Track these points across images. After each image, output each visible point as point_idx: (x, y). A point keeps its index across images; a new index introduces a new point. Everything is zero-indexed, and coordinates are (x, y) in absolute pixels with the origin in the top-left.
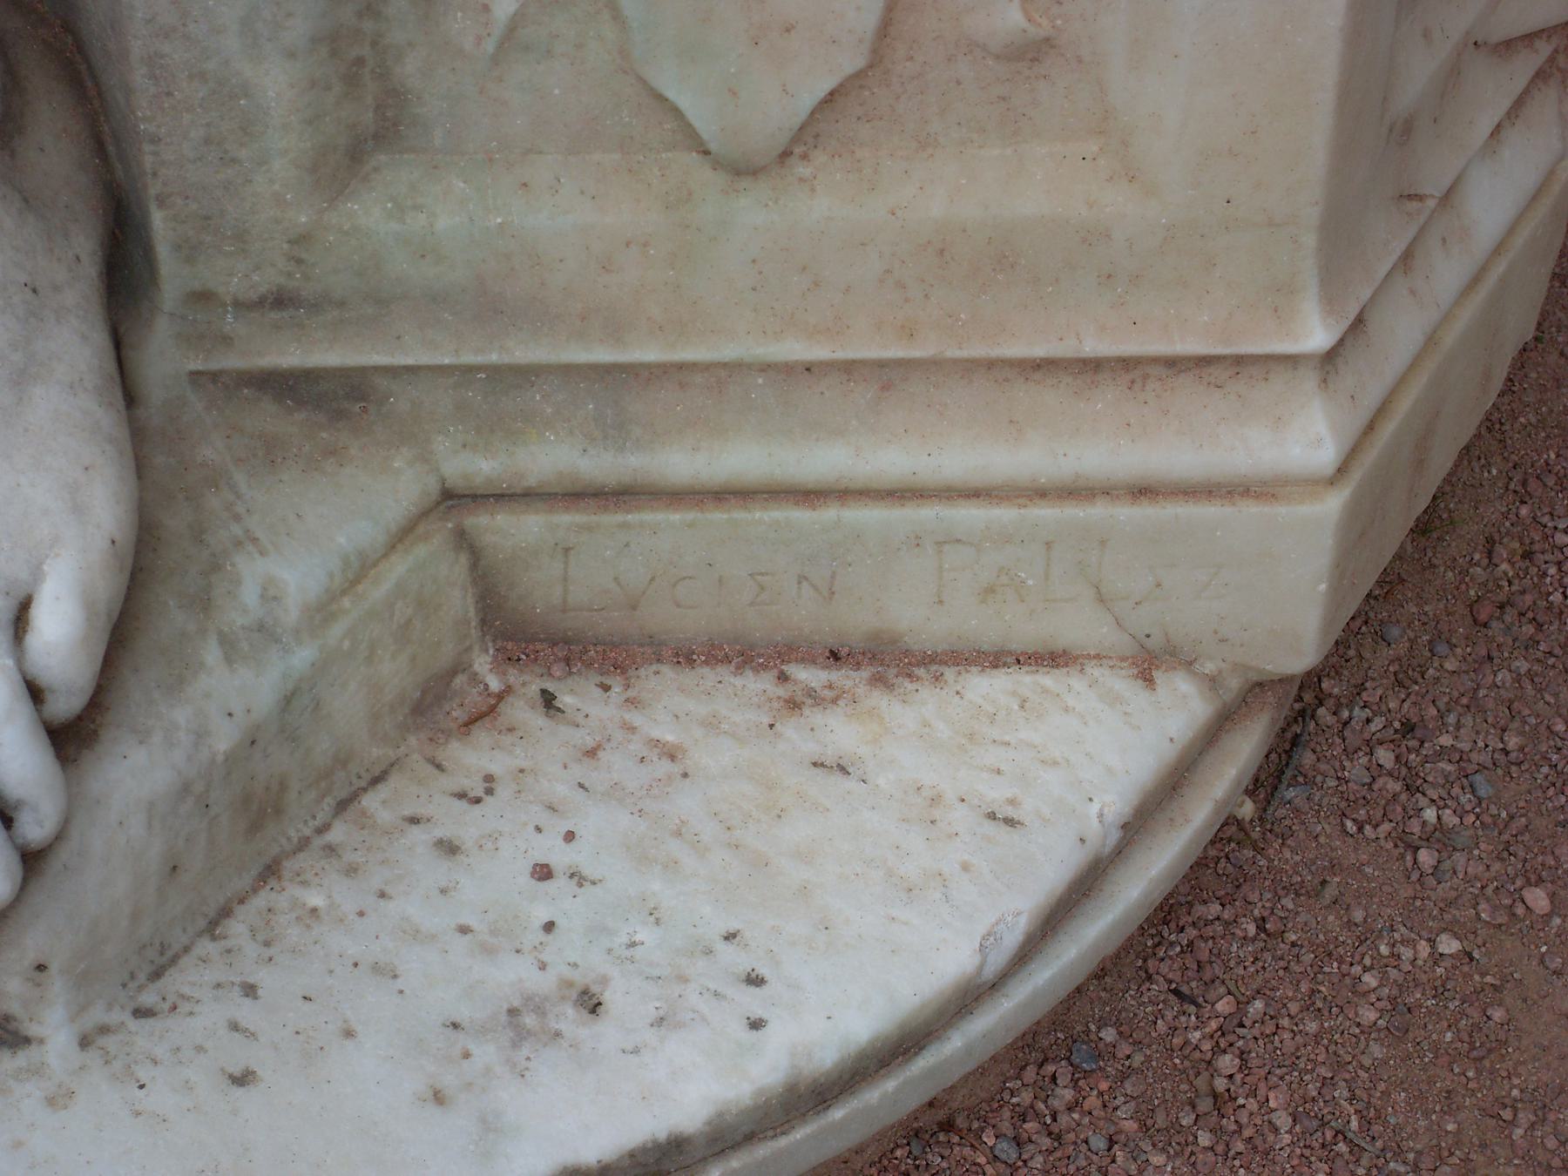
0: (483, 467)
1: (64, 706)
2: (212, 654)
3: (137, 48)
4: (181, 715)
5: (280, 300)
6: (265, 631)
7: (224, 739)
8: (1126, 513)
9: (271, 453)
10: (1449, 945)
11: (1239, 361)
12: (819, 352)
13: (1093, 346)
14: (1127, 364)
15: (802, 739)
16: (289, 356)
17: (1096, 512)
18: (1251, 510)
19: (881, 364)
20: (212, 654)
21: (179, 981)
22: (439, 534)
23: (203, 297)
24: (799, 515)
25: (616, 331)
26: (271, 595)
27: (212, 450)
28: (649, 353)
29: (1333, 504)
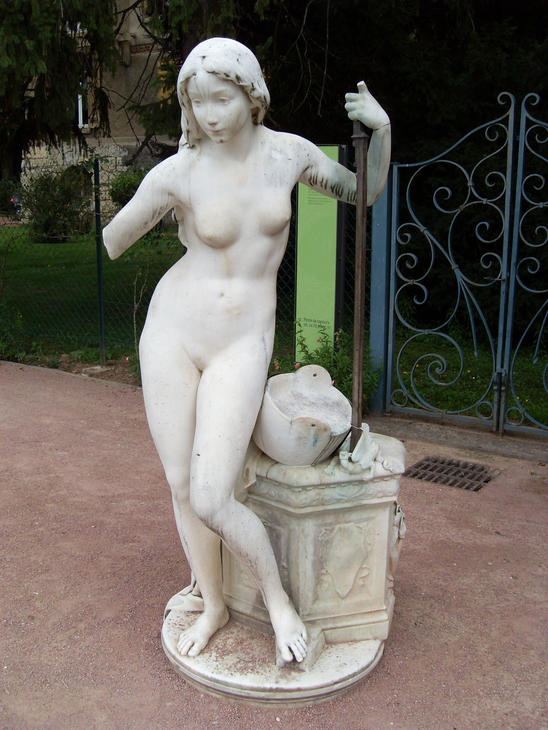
0: (325, 627)
1: (306, 641)
2: (312, 640)
3: (300, 593)
5: (309, 615)
8: (373, 624)
10: (401, 662)
11: (379, 610)
12: (349, 614)
14: (371, 612)
15: (352, 647)
16: (310, 619)
17: (371, 625)
18: (382, 623)
19: (354, 614)
20: (312, 640)
21: (314, 666)
23: (303, 615)
25: (334, 614)
26: (314, 636)
28: (336, 615)
29: (388, 622)
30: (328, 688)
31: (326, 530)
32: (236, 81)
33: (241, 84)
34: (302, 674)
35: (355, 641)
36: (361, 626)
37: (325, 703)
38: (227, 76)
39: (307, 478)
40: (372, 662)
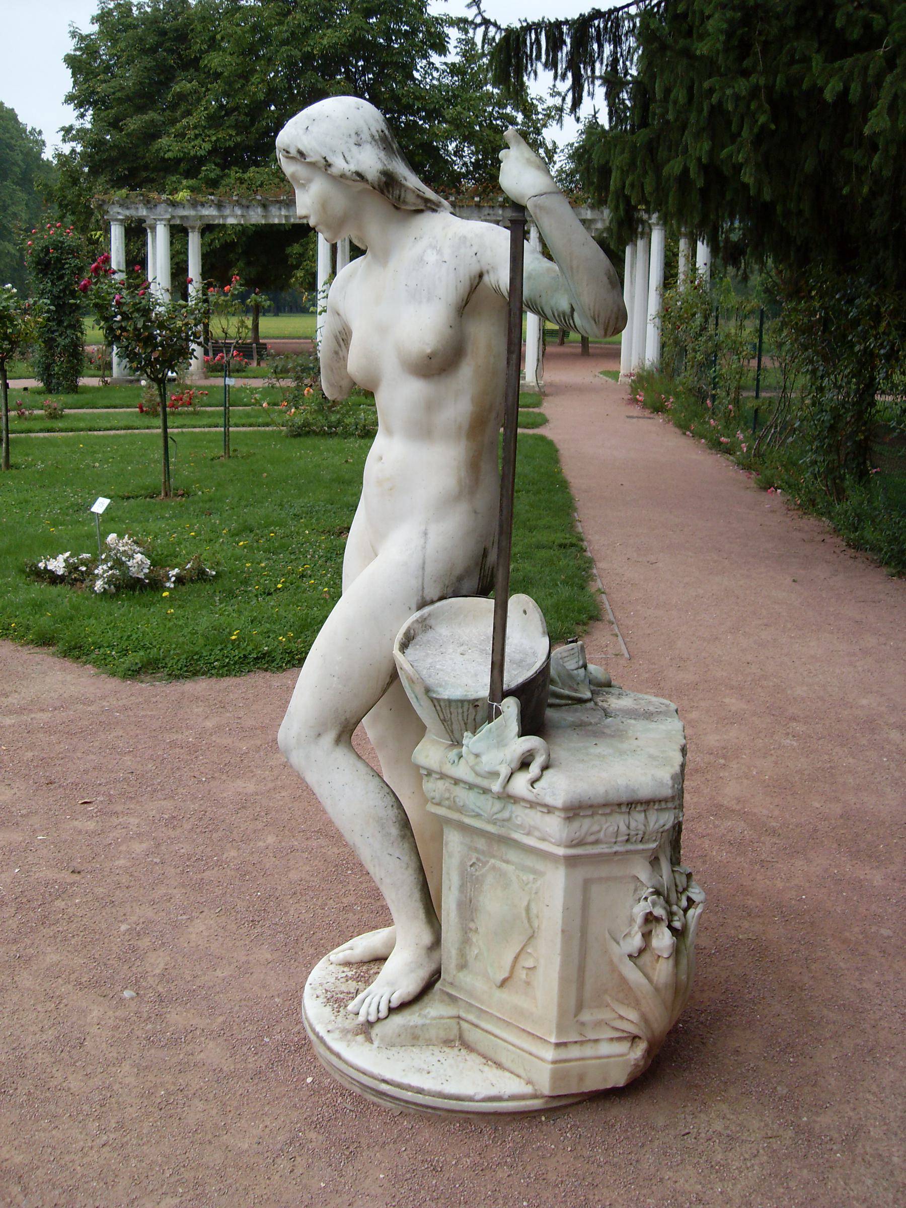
0: (463, 1015)
4: (409, 1018)
5: (452, 984)
6: (425, 1016)
7: (412, 1023)
8: (527, 1056)
9: (442, 1001)
13: (529, 1030)
16: (453, 993)
17: (524, 1053)
18: (540, 1062)
22: (454, 1021)
24: (493, 1038)
26: (429, 1013)
27: (437, 997)
30: (371, 1080)
31: (478, 859)
32: (298, 157)
33: (308, 160)
34: (367, 1044)
35: (499, 1065)
36: (510, 1047)
37: (374, 1104)
38: (288, 152)
39: (427, 757)
40: (471, 1099)
